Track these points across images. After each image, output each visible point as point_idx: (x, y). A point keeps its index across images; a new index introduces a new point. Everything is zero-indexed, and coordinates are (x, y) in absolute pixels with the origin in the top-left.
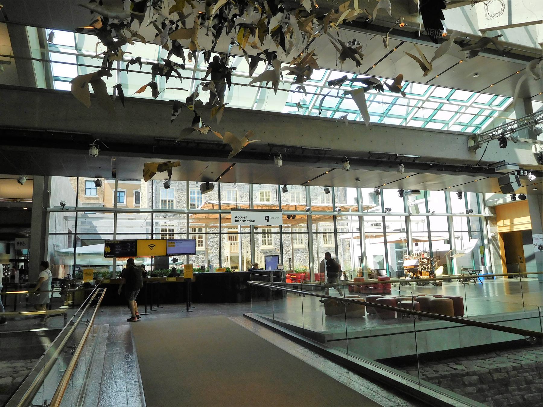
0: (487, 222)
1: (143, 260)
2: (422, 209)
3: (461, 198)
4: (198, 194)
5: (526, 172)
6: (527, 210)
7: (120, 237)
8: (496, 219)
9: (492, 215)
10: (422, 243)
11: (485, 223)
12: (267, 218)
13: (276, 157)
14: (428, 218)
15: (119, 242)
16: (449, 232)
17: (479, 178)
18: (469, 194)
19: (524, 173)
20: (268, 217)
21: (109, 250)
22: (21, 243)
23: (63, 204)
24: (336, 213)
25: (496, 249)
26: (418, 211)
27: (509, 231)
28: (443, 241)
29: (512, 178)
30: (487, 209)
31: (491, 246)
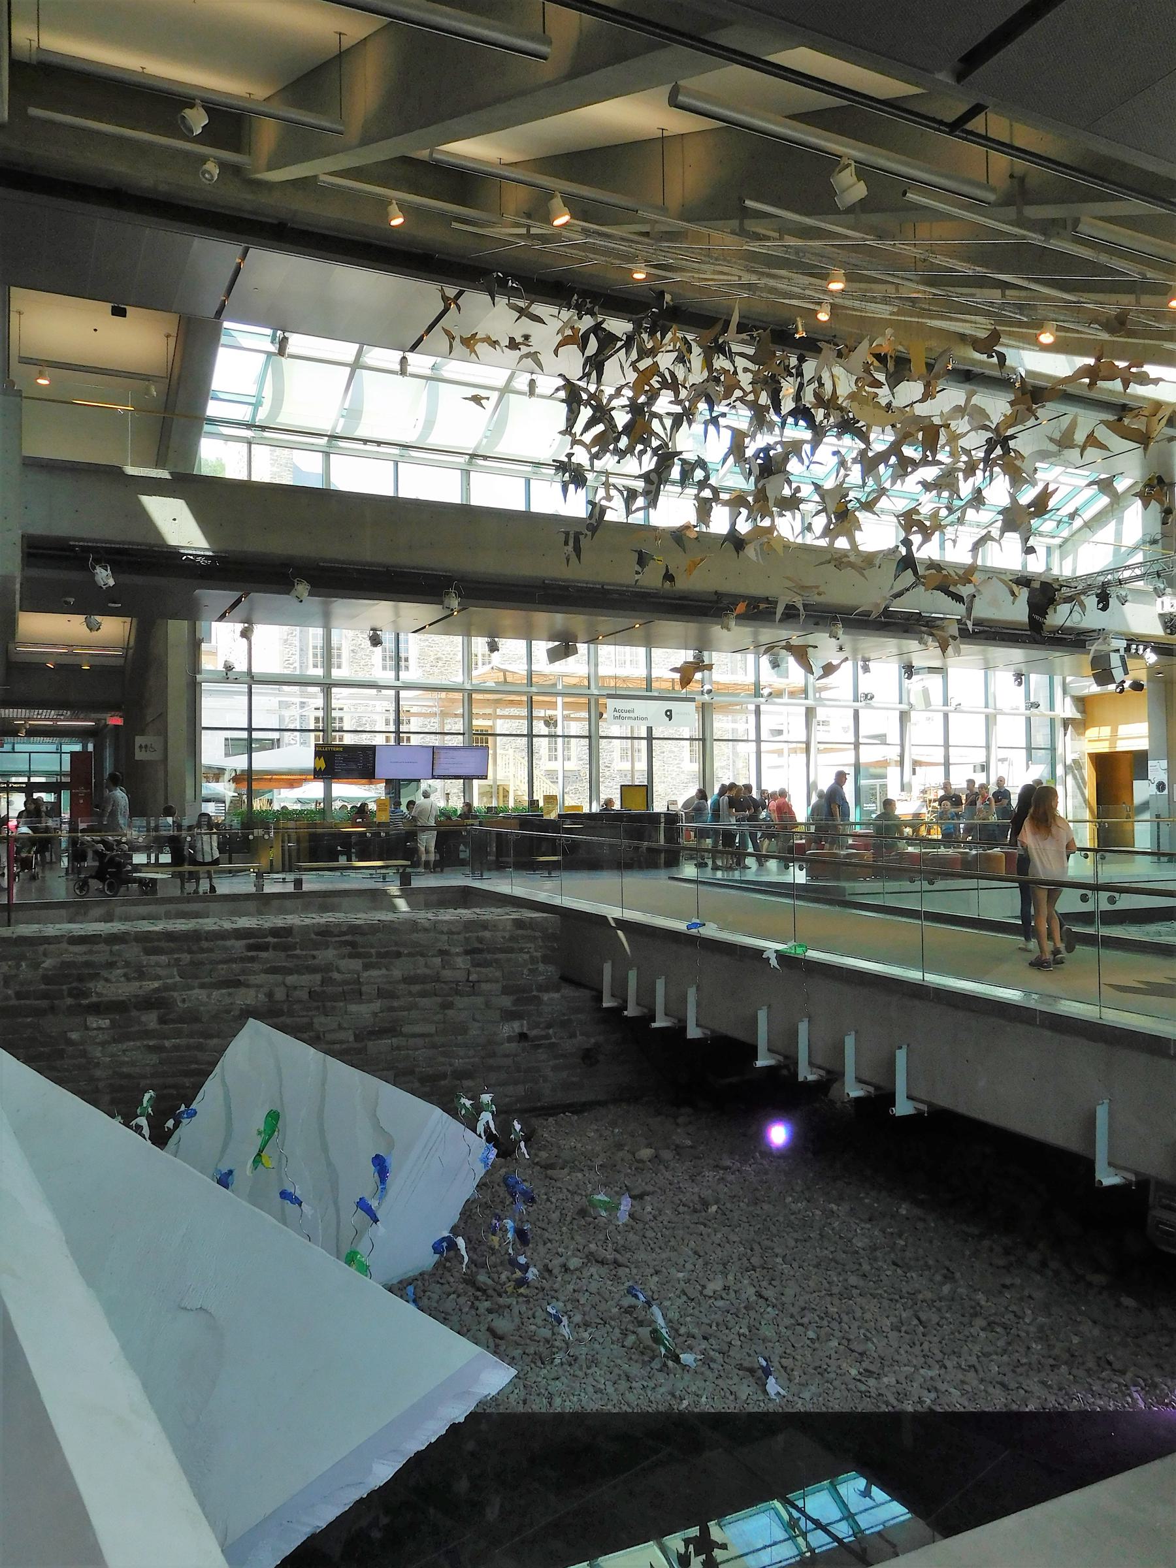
0: (1066, 729)
2: (937, 699)
3: (1020, 684)
4: (483, 655)
5: (1141, 648)
6: (1145, 712)
8: (1085, 724)
9: (1078, 716)
10: (923, 768)
11: (1062, 729)
13: (726, 615)
14: (946, 716)
16: (988, 747)
17: (1058, 654)
18: (1034, 678)
19: (1137, 650)
20: (670, 711)
21: (322, 764)
22: (146, 746)
23: (229, 668)
25: (1080, 787)
26: (928, 703)
27: (1107, 750)
28: (972, 766)
29: (1115, 660)
30: (1068, 700)
31: (1070, 779)
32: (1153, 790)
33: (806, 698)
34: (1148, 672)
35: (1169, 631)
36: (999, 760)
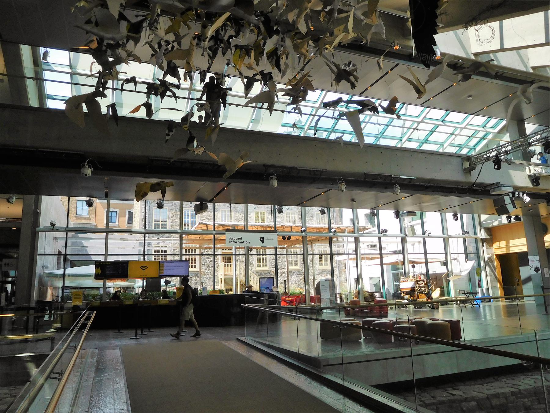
0: (483, 244)
1: (135, 282)
3: (457, 219)
4: (192, 214)
5: (521, 194)
7: (111, 259)
9: (488, 237)
11: (481, 244)
12: (262, 239)
14: (424, 239)
15: (110, 264)
16: (446, 253)
17: (474, 199)
19: (518, 195)
20: (263, 238)
21: (99, 271)
22: (8, 264)
24: (332, 234)
25: (493, 271)
26: (414, 232)
27: (505, 253)
30: (483, 230)
31: (488, 268)
32: (533, 272)
33: (355, 233)
34: (522, 210)
35: (535, 184)
36: (453, 260)
